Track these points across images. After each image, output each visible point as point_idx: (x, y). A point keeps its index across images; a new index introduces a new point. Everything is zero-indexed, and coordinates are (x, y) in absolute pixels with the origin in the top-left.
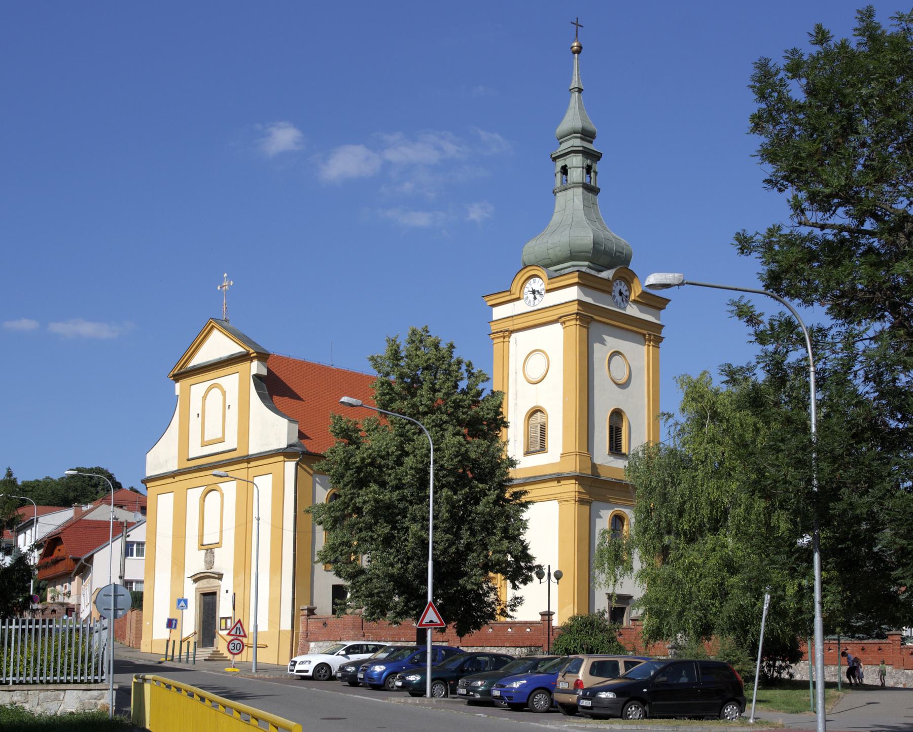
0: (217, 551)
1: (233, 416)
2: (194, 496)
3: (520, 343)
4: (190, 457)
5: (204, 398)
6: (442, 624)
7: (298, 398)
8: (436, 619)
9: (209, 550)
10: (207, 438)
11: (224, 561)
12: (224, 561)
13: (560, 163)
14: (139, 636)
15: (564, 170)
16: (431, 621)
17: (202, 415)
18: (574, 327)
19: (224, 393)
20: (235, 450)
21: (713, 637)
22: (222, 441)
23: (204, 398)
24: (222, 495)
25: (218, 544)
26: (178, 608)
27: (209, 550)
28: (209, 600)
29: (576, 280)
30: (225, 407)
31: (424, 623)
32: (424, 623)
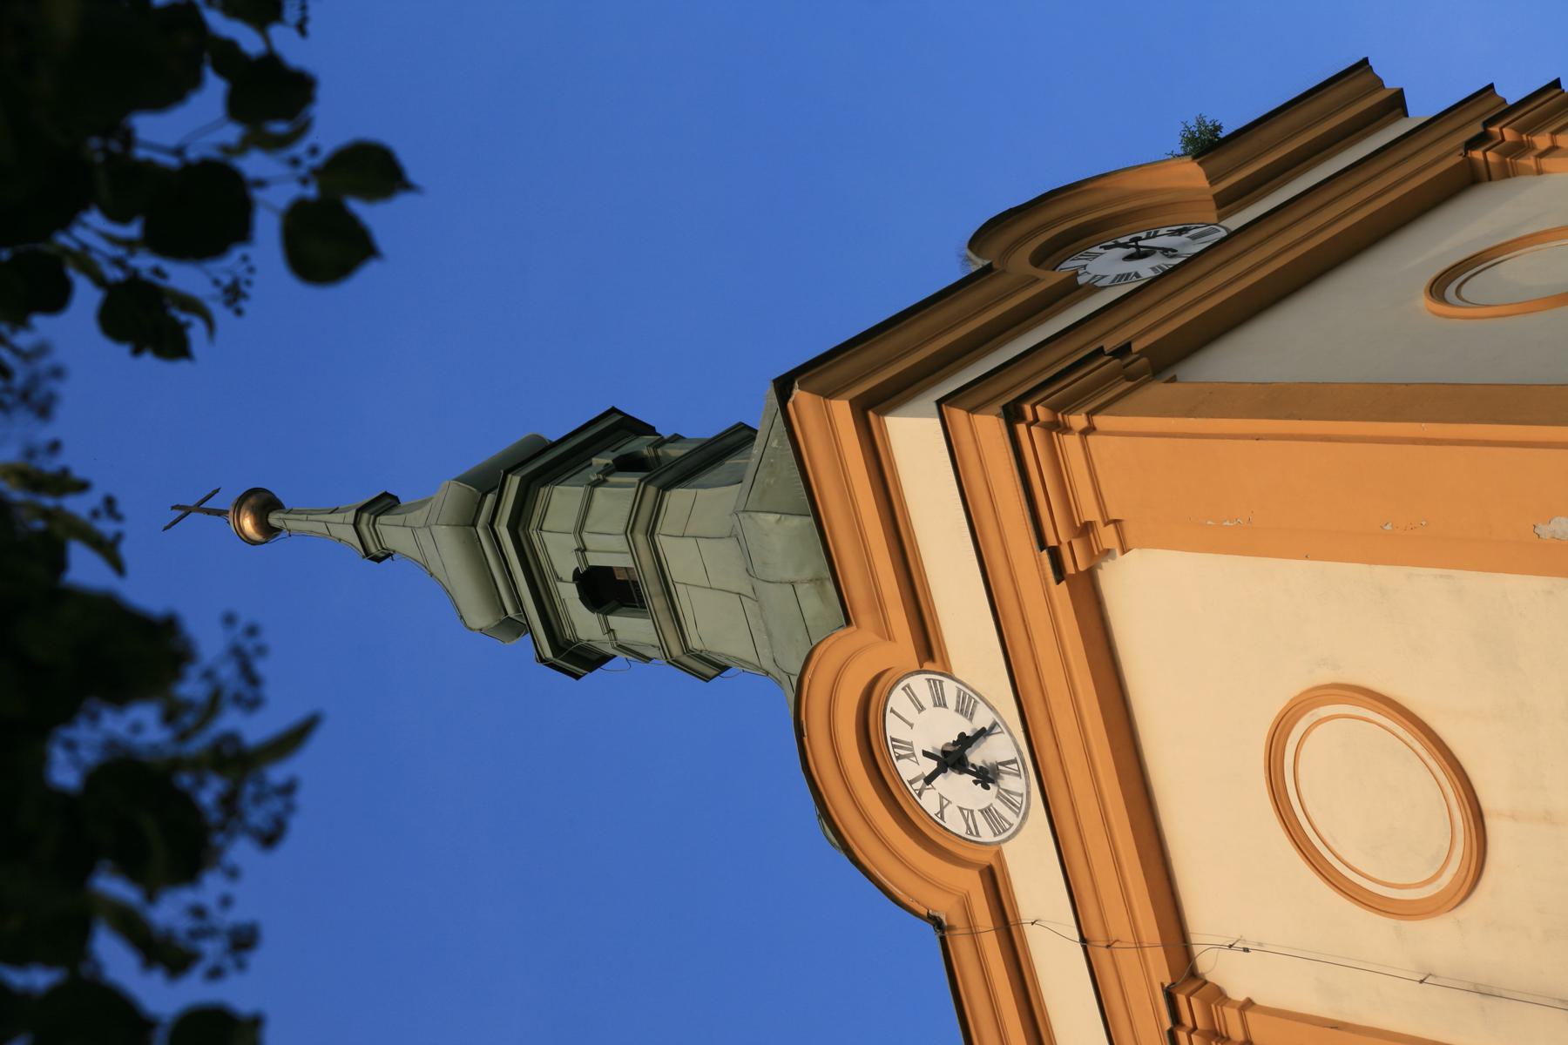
3: (1256, 924)
13: (585, 624)
15: (605, 590)
18: (1119, 453)
29: (841, 409)
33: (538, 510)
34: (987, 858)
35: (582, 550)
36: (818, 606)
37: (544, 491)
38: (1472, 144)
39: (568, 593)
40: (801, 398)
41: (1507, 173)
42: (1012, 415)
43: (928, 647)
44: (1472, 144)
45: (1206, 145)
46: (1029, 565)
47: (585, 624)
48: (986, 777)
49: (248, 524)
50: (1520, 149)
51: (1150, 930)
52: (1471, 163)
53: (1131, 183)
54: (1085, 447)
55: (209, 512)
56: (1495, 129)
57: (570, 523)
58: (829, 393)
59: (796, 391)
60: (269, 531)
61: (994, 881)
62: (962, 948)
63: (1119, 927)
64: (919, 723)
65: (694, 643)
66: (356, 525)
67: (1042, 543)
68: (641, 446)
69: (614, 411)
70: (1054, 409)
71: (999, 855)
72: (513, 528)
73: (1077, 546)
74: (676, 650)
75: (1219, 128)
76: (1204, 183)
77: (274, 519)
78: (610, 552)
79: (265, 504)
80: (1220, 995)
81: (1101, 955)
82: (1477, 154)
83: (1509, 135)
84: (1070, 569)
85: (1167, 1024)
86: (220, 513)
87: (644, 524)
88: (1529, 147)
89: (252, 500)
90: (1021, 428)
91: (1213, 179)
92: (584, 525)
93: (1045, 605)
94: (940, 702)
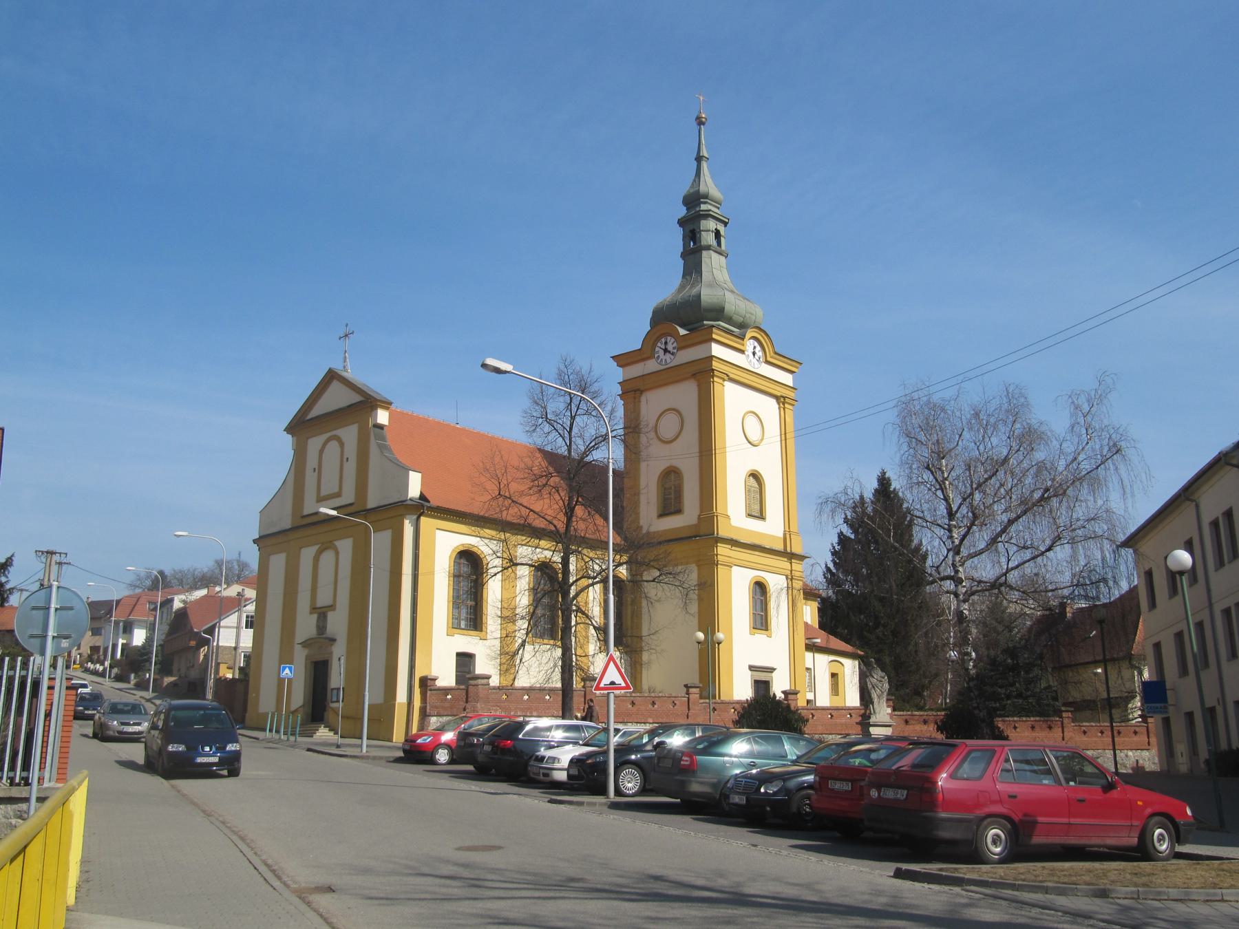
0: (330, 615)
1: (351, 468)
2: (308, 554)
4: (305, 513)
5: (321, 451)
6: (627, 687)
7: (500, 848)
8: (619, 680)
9: (322, 614)
10: (323, 493)
11: (338, 623)
12: (338, 623)
14: (245, 710)
16: (613, 683)
17: (319, 470)
19: (342, 444)
20: (351, 504)
21: (821, 579)
22: (338, 495)
23: (321, 451)
24: (337, 553)
25: (332, 607)
26: (234, 773)
27: (322, 614)
28: (319, 671)
30: (343, 460)
31: (602, 685)
32: (602, 685)
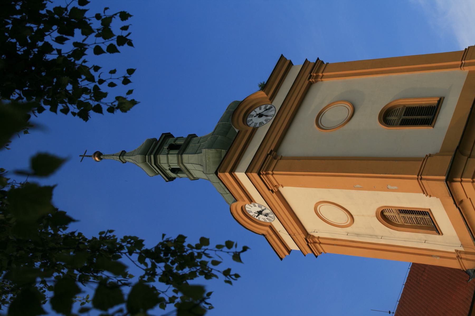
13: (173, 175)
29: (227, 174)
33: (158, 160)
34: (270, 224)
35: (169, 166)
36: (228, 197)
37: (158, 156)
38: (309, 79)
39: (169, 172)
40: (220, 174)
41: (316, 82)
42: (259, 174)
43: (251, 200)
44: (309, 79)
45: (263, 87)
46: (268, 193)
47: (173, 175)
48: (266, 215)
49: (97, 159)
50: (317, 77)
51: (300, 231)
52: (310, 82)
53: (253, 97)
54: (273, 177)
55: (87, 156)
56: (312, 74)
57: (166, 162)
58: (224, 172)
59: (219, 173)
60: (101, 159)
61: (271, 227)
62: (269, 238)
63: (294, 231)
64: (252, 209)
65: (195, 177)
66: (120, 159)
67: (269, 190)
68: (171, 141)
69: (163, 134)
70: (265, 171)
71: (271, 224)
72: (155, 164)
73: (275, 188)
74: (192, 178)
75: (264, 82)
76: (265, 96)
77: (102, 157)
78: (175, 166)
79: (99, 154)
80: (313, 237)
81: (294, 237)
82: (311, 80)
83: (315, 75)
84: (274, 191)
85: (269, 153)
86: (90, 156)
87: (181, 161)
88: (319, 75)
89: (96, 155)
90: (261, 176)
91: (267, 94)
92: (168, 160)
93: (274, 198)
94: (255, 206)
